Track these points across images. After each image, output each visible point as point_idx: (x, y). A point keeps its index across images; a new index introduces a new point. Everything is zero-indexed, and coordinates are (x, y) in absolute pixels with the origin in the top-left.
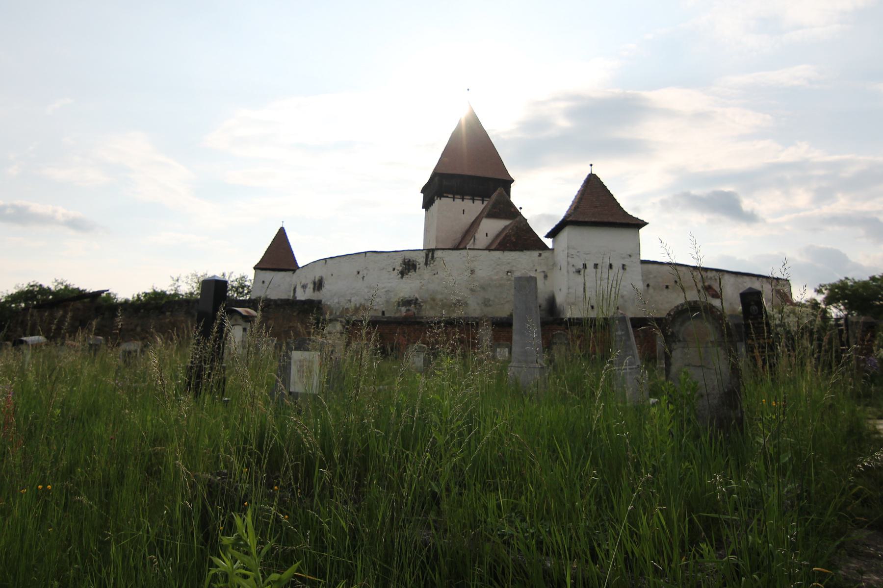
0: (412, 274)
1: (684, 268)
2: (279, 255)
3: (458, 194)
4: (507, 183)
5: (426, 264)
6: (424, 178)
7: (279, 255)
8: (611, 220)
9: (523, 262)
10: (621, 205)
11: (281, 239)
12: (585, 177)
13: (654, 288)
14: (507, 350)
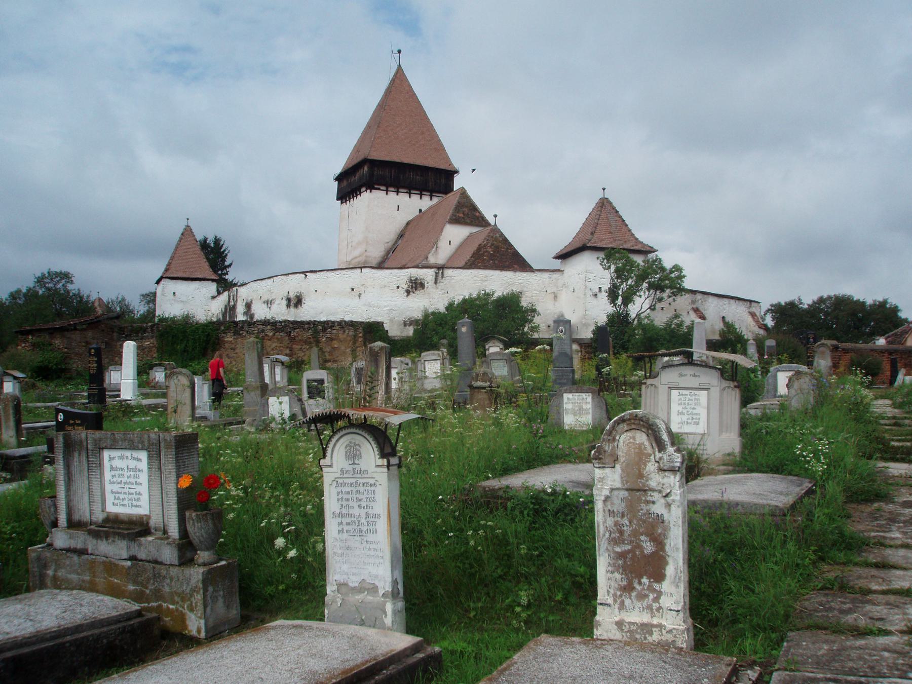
0: (420, 292)
3: (391, 186)
5: (436, 282)
8: (200, 276)
9: (498, 283)
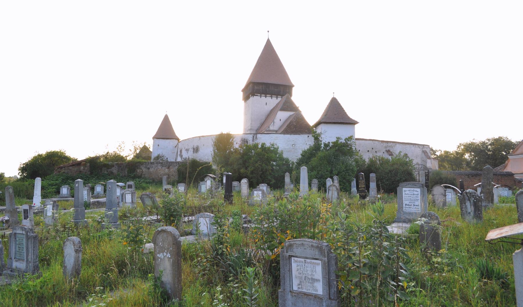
1: (377, 142)
2: (165, 131)
6: (243, 86)
7: (165, 131)
12: (330, 99)
14: (292, 258)
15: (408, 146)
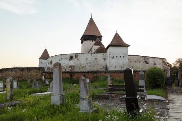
2: (45, 56)
4: (100, 37)
5: (75, 57)
7: (45, 56)
10: (124, 41)
11: (46, 51)
13: (132, 62)
15: (156, 59)
